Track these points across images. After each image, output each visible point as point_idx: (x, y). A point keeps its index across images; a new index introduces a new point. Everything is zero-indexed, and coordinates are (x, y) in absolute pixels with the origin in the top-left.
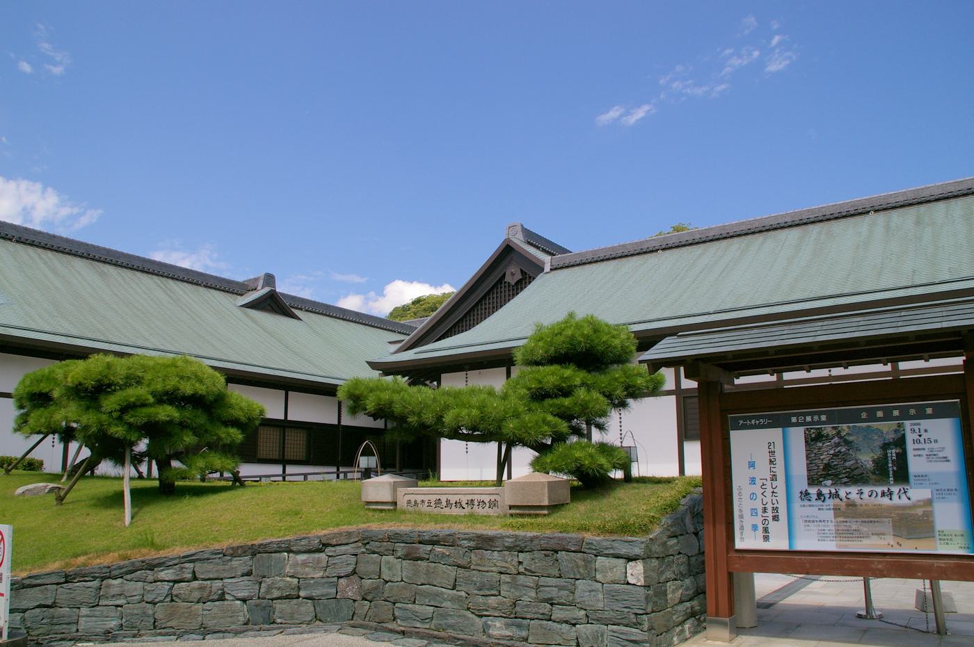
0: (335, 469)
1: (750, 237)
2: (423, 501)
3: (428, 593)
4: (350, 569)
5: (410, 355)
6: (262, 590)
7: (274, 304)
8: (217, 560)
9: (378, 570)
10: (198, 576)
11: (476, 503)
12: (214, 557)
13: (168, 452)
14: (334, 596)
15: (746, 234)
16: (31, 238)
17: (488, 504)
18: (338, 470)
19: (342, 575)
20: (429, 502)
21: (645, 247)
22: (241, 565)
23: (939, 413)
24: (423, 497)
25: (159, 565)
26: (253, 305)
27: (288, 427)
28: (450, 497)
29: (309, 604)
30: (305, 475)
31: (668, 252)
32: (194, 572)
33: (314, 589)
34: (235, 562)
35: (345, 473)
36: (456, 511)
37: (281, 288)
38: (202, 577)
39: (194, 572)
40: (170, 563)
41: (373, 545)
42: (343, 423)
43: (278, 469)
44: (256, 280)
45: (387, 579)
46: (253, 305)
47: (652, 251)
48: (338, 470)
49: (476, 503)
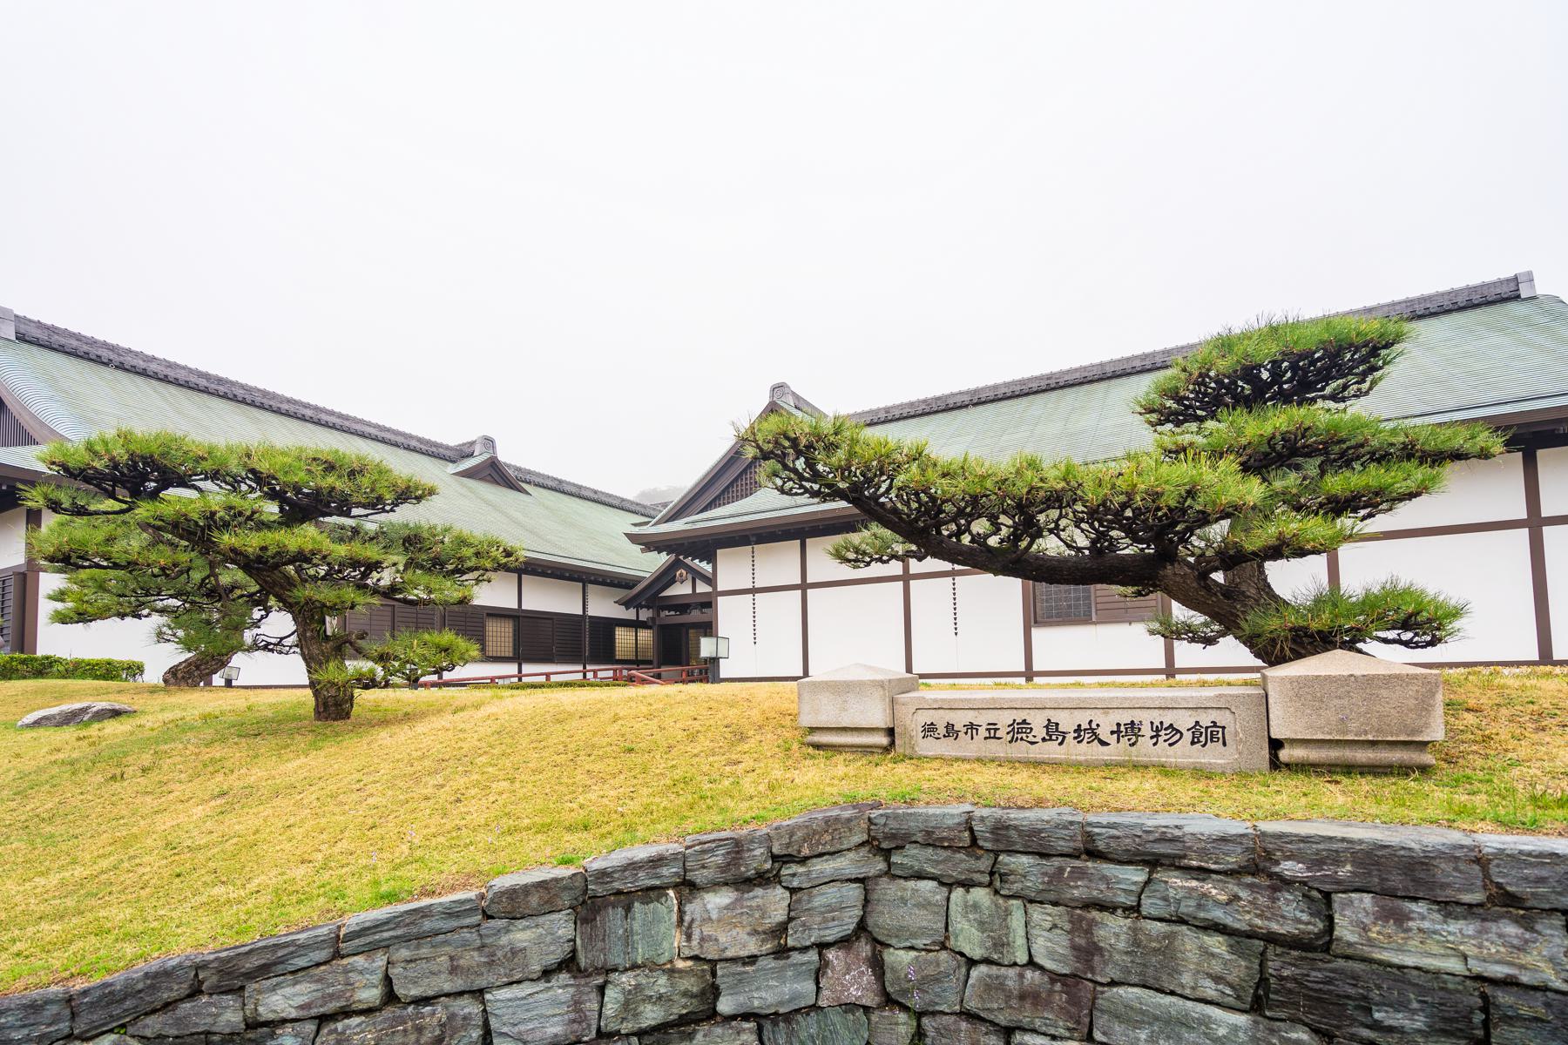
0: (580, 668)
1: (1086, 387)
2: (972, 727)
3: (1143, 1012)
4: (849, 922)
5: (678, 526)
6: (610, 1009)
7: (495, 473)
8: (466, 934)
9: (941, 925)
10: (400, 991)
11: (1146, 731)
12: (454, 923)
13: (1040, 941)
14: (812, 1002)
15: (1081, 384)
16: (141, 364)
17: (1188, 736)
18: (520, 671)
19: (830, 939)
20: (993, 729)
21: (951, 402)
22: (539, 942)
23: (698, 643)
24: (970, 717)
25: (264, 971)
26: (468, 474)
27: (596, 582)
28: (1098, 717)
29: (744, 1037)
30: (548, 675)
31: (980, 408)
32: (388, 980)
33: (758, 989)
34: (522, 935)
35: (595, 672)
36: (1076, 750)
37: (504, 456)
38: (415, 992)
39: (388, 980)
40: (301, 962)
41: (908, 858)
42: (591, 612)
43: (512, 669)
44: (472, 443)
45: (977, 953)
46: (468, 474)
47: (960, 407)
48: (520, 671)
49: (1146, 731)
